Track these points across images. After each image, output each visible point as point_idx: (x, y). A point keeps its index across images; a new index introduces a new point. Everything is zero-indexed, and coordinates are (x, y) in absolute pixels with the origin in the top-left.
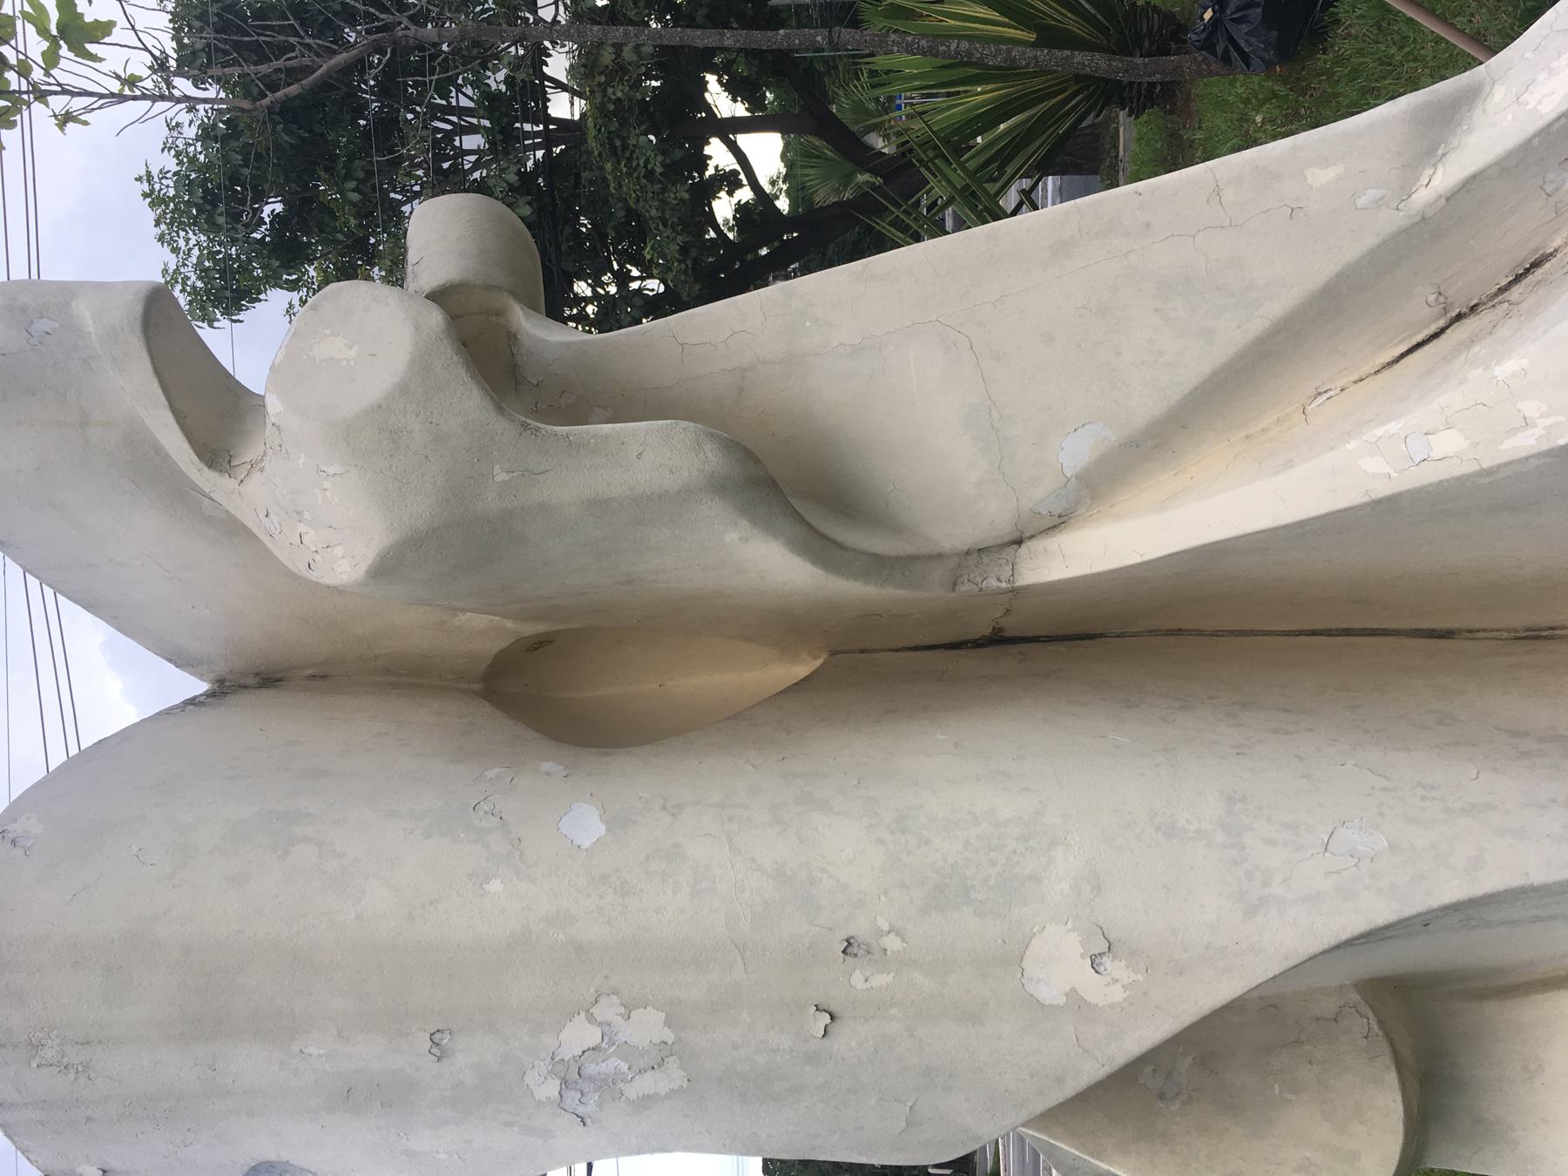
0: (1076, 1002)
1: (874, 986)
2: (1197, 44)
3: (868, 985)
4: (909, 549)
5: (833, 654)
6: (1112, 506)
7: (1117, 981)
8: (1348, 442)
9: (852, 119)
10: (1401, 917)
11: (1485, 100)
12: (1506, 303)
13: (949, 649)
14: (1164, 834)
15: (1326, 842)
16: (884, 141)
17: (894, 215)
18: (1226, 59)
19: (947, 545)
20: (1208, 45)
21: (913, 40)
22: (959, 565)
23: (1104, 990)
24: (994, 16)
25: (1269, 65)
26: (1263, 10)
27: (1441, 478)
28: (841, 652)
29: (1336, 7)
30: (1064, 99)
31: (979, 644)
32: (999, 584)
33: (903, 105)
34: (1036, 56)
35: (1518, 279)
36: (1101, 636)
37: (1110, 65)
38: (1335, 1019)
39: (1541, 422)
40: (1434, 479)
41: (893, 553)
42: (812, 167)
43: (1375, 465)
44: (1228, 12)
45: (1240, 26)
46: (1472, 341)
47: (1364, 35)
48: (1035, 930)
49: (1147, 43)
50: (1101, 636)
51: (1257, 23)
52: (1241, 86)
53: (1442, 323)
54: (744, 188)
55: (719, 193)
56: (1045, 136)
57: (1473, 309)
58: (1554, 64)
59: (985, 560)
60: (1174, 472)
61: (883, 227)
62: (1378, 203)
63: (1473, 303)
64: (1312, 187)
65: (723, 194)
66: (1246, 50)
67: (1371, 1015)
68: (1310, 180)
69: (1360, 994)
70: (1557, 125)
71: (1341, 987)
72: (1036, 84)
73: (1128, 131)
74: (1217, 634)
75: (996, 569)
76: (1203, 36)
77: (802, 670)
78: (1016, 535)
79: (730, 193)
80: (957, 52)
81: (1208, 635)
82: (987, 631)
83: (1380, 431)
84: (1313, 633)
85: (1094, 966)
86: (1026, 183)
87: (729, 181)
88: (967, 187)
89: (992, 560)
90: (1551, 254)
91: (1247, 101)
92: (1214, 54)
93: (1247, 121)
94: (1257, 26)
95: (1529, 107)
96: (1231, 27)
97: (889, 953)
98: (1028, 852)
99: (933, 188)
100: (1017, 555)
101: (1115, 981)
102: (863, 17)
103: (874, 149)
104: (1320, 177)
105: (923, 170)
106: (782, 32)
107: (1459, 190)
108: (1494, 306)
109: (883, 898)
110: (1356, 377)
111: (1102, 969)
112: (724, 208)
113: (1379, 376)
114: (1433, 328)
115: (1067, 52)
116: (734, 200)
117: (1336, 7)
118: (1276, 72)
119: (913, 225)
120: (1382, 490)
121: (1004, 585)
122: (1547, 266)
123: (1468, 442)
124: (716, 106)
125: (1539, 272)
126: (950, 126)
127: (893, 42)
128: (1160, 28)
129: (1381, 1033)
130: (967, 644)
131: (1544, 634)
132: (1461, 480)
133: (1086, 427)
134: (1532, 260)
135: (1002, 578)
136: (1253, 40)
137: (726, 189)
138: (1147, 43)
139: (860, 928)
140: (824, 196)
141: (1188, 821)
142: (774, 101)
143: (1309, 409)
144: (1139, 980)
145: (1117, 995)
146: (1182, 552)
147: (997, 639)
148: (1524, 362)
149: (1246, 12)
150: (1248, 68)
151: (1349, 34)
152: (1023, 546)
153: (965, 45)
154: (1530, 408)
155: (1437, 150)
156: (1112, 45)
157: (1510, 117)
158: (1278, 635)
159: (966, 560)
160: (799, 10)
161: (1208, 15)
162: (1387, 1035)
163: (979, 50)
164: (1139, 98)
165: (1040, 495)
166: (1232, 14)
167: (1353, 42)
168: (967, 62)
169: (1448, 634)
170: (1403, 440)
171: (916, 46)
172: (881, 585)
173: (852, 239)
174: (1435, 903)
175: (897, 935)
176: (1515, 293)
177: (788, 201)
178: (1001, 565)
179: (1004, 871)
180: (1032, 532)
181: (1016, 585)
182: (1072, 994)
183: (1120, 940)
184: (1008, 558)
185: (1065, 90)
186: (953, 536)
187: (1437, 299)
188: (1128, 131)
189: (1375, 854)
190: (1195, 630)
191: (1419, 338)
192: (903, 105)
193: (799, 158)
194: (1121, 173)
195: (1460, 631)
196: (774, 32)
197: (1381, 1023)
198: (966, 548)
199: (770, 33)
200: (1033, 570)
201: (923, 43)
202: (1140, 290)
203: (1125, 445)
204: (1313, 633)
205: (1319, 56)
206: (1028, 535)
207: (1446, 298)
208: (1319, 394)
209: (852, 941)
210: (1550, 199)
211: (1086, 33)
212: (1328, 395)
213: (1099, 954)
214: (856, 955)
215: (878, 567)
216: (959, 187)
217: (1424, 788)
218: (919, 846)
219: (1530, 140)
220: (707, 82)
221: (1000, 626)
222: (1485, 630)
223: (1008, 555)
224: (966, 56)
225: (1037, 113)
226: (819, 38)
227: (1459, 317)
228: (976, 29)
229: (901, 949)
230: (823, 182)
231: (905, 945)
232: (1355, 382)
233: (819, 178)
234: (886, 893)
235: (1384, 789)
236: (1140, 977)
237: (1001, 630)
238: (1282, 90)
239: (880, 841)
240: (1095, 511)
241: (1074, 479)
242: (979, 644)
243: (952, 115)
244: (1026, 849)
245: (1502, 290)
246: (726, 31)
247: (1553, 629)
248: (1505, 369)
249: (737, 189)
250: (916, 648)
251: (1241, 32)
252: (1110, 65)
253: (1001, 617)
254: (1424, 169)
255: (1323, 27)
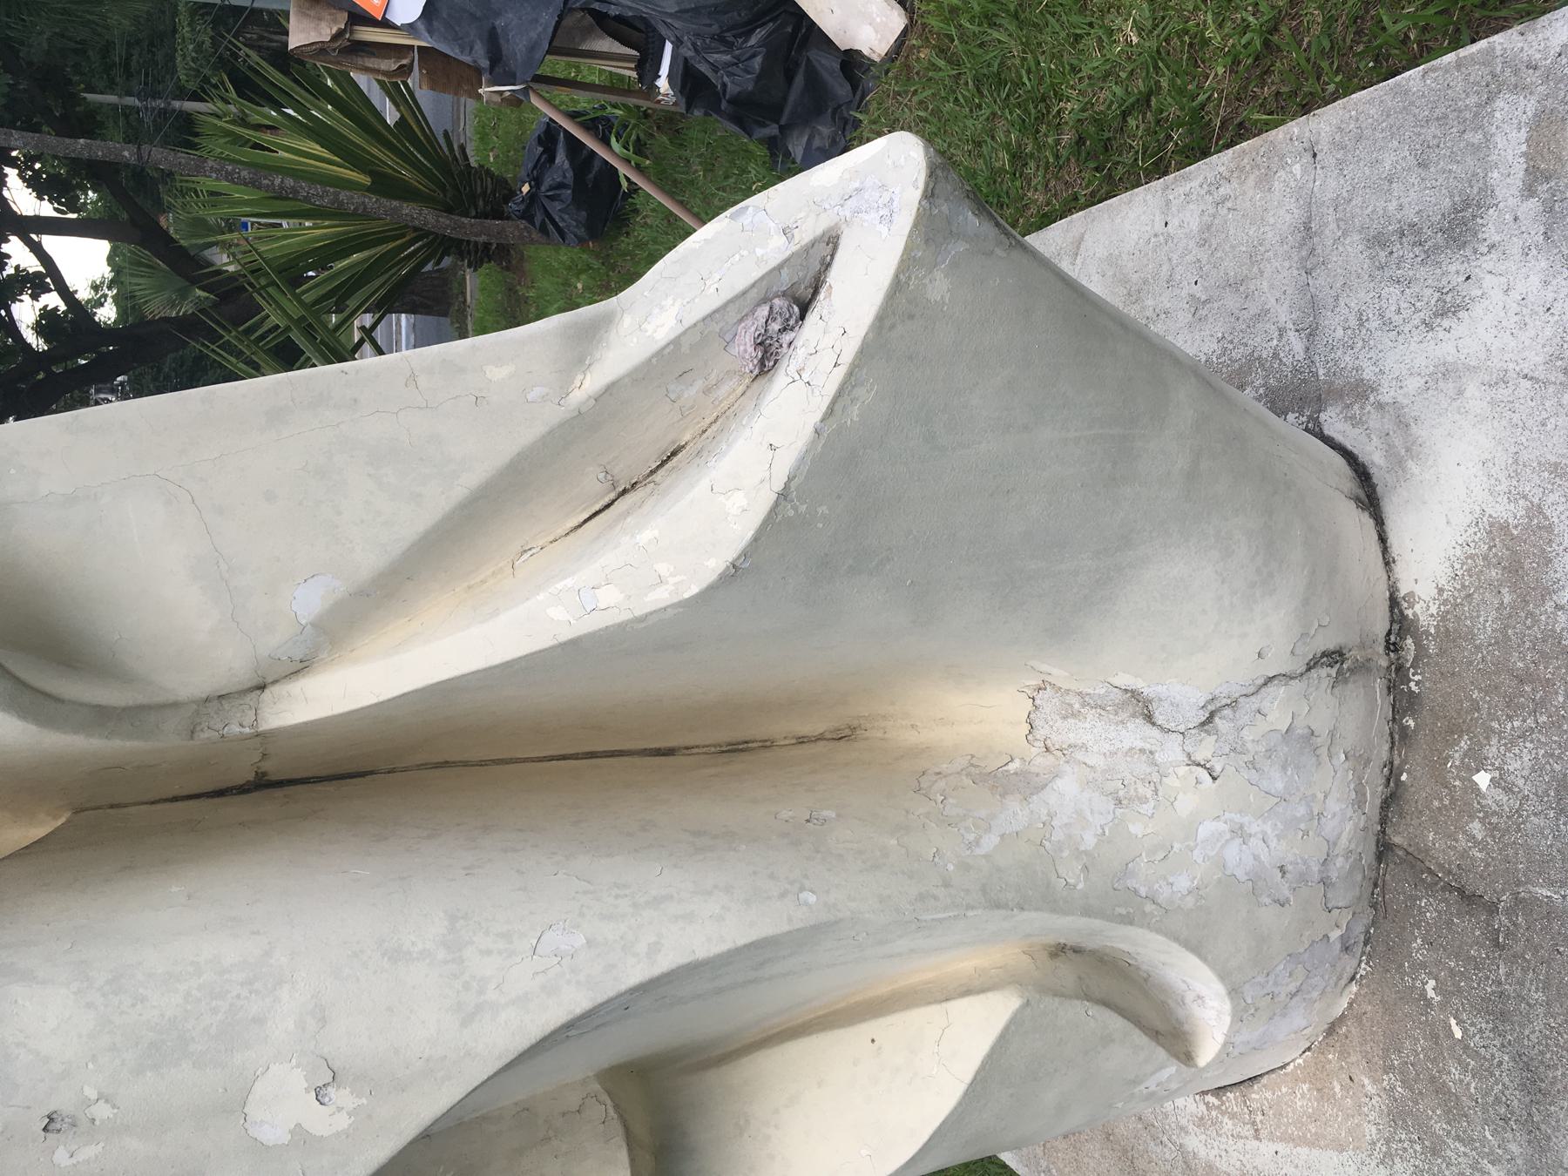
0: (301, 1137)
1: (81, 1160)
2: (517, 213)
3: (74, 1161)
4: (141, 699)
5: (78, 811)
6: (352, 651)
7: (343, 1108)
8: (538, 594)
9: (189, 232)
10: (596, 1004)
11: (618, 324)
12: (653, 484)
13: (212, 797)
14: (389, 959)
15: (534, 945)
16: (228, 257)
17: (217, 344)
18: (543, 230)
19: (184, 693)
20: (527, 216)
21: (234, 170)
22: (197, 712)
23: (325, 1122)
24: (326, 154)
25: (581, 241)
26: (573, 192)
27: (607, 625)
28: (87, 809)
29: (634, 198)
30: (402, 245)
31: (243, 789)
32: (242, 730)
33: (249, 224)
34: (363, 203)
35: (663, 463)
36: (372, 773)
37: (437, 221)
38: (578, 1111)
39: (672, 580)
40: (602, 625)
41: (122, 703)
42: (142, 276)
43: (558, 613)
44: (543, 189)
45: (553, 203)
46: (628, 513)
47: (657, 226)
48: (258, 1073)
49: (481, 203)
50: (372, 773)
51: (568, 202)
52: (564, 255)
53: (612, 496)
54: (52, 293)
55: (21, 294)
56: (387, 276)
57: (634, 485)
58: (664, 303)
59: (226, 706)
60: (408, 619)
61: (213, 350)
62: (544, 398)
63: (634, 481)
64: (491, 381)
65: (25, 297)
66: (561, 225)
67: (609, 1102)
68: (488, 375)
69: (600, 1084)
70: (668, 350)
71: (584, 1080)
72: (374, 226)
73: (474, 283)
74: (482, 763)
75: (239, 715)
76: (522, 207)
77: (39, 832)
78: (260, 681)
79: (35, 297)
80: (281, 188)
81: (473, 765)
82: (251, 777)
83: (560, 586)
84: (564, 757)
85: (319, 1098)
86: (368, 320)
87: (33, 285)
88: (303, 318)
89: (233, 706)
90: (683, 447)
91: (569, 268)
92: (533, 224)
93: (570, 286)
94: (569, 205)
95: (648, 334)
96: (546, 202)
97: (97, 1123)
98: (253, 995)
99: (268, 316)
100: (260, 700)
101: (340, 1109)
102: (202, 131)
103: (213, 265)
104: (497, 373)
105: (255, 295)
106: (82, 141)
107: (604, 393)
108: (645, 485)
109: (91, 1066)
110: (551, 539)
111: (327, 1099)
112: (25, 312)
113: (568, 537)
114: (606, 500)
115: (395, 203)
116: (39, 305)
117: (634, 198)
118: (589, 247)
119: (246, 351)
120: (566, 635)
121: (247, 730)
122: (680, 455)
123: (623, 595)
124: (14, 203)
125: (675, 459)
126: (282, 256)
127: (212, 168)
128: (494, 192)
129: (616, 1116)
130: (232, 790)
131: (741, 747)
132: (622, 626)
133: (315, 577)
134: (672, 450)
135: (244, 723)
136: (566, 217)
137: (29, 292)
138: (481, 203)
139: (62, 1102)
140: (158, 307)
141: (413, 943)
142: (97, 201)
143: (517, 563)
144: (363, 1104)
145: (343, 1122)
146: (413, 692)
147: (262, 784)
148: (656, 533)
149: (558, 192)
150: (563, 240)
151: (646, 223)
152: (267, 691)
153: (290, 182)
154: (663, 568)
155: (585, 361)
156: (448, 200)
157: (635, 340)
158: (533, 761)
159: (206, 707)
160: (128, 111)
161: (526, 188)
162: (621, 1117)
163: (304, 188)
164: (480, 255)
165: (276, 641)
166: (548, 191)
167: (648, 230)
168: (344, 188)
169: (670, 752)
170: (577, 593)
171: (236, 176)
172: (107, 737)
173: (193, 355)
174: (623, 988)
175: (107, 1101)
176: (658, 477)
177: (115, 309)
178: (243, 711)
179: (227, 1018)
180: (276, 677)
181: (261, 729)
182: (298, 1132)
183: (344, 1069)
184: (251, 703)
185: (403, 236)
186: (193, 684)
187: (605, 477)
188: (474, 283)
189: (576, 951)
190: (460, 762)
191: (597, 507)
192: (249, 224)
193: (127, 266)
194: (469, 318)
195: (679, 749)
196: (73, 140)
197: (616, 1107)
198: (204, 696)
199: (67, 141)
200: (277, 714)
201: (244, 173)
202: (352, 457)
203: (355, 594)
204: (564, 757)
205: (622, 238)
206: (271, 680)
207: (612, 476)
208: (525, 551)
209: (54, 1116)
210: (675, 404)
211: (422, 185)
212: (530, 553)
213: (324, 1085)
214: (59, 1131)
215: (102, 717)
216: (296, 318)
217: (618, 888)
218: (133, 1005)
219: (649, 360)
220: (6, 175)
221: (263, 770)
222: (697, 747)
223: (251, 700)
224: (291, 193)
225: (374, 256)
226: (126, 153)
227: (625, 492)
228: (311, 165)
229: (111, 1116)
230: (155, 293)
231: (116, 1111)
232: (551, 542)
233: (150, 289)
234: (94, 1058)
235: (585, 893)
236: (364, 1101)
237: (264, 774)
238: (596, 264)
239: (89, 1005)
240: (337, 655)
241: (309, 626)
242: (243, 789)
243: (289, 245)
244: (251, 993)
245: (653, 472)
246: (14, 131)
247: (746, 742)
248: (645, 536)
249: (44, 293)
250: (175, 799)
251: (555, 208)
252: (437, 221)
253: (260, 761)
254: (576, 375)
255: (624, 214)
